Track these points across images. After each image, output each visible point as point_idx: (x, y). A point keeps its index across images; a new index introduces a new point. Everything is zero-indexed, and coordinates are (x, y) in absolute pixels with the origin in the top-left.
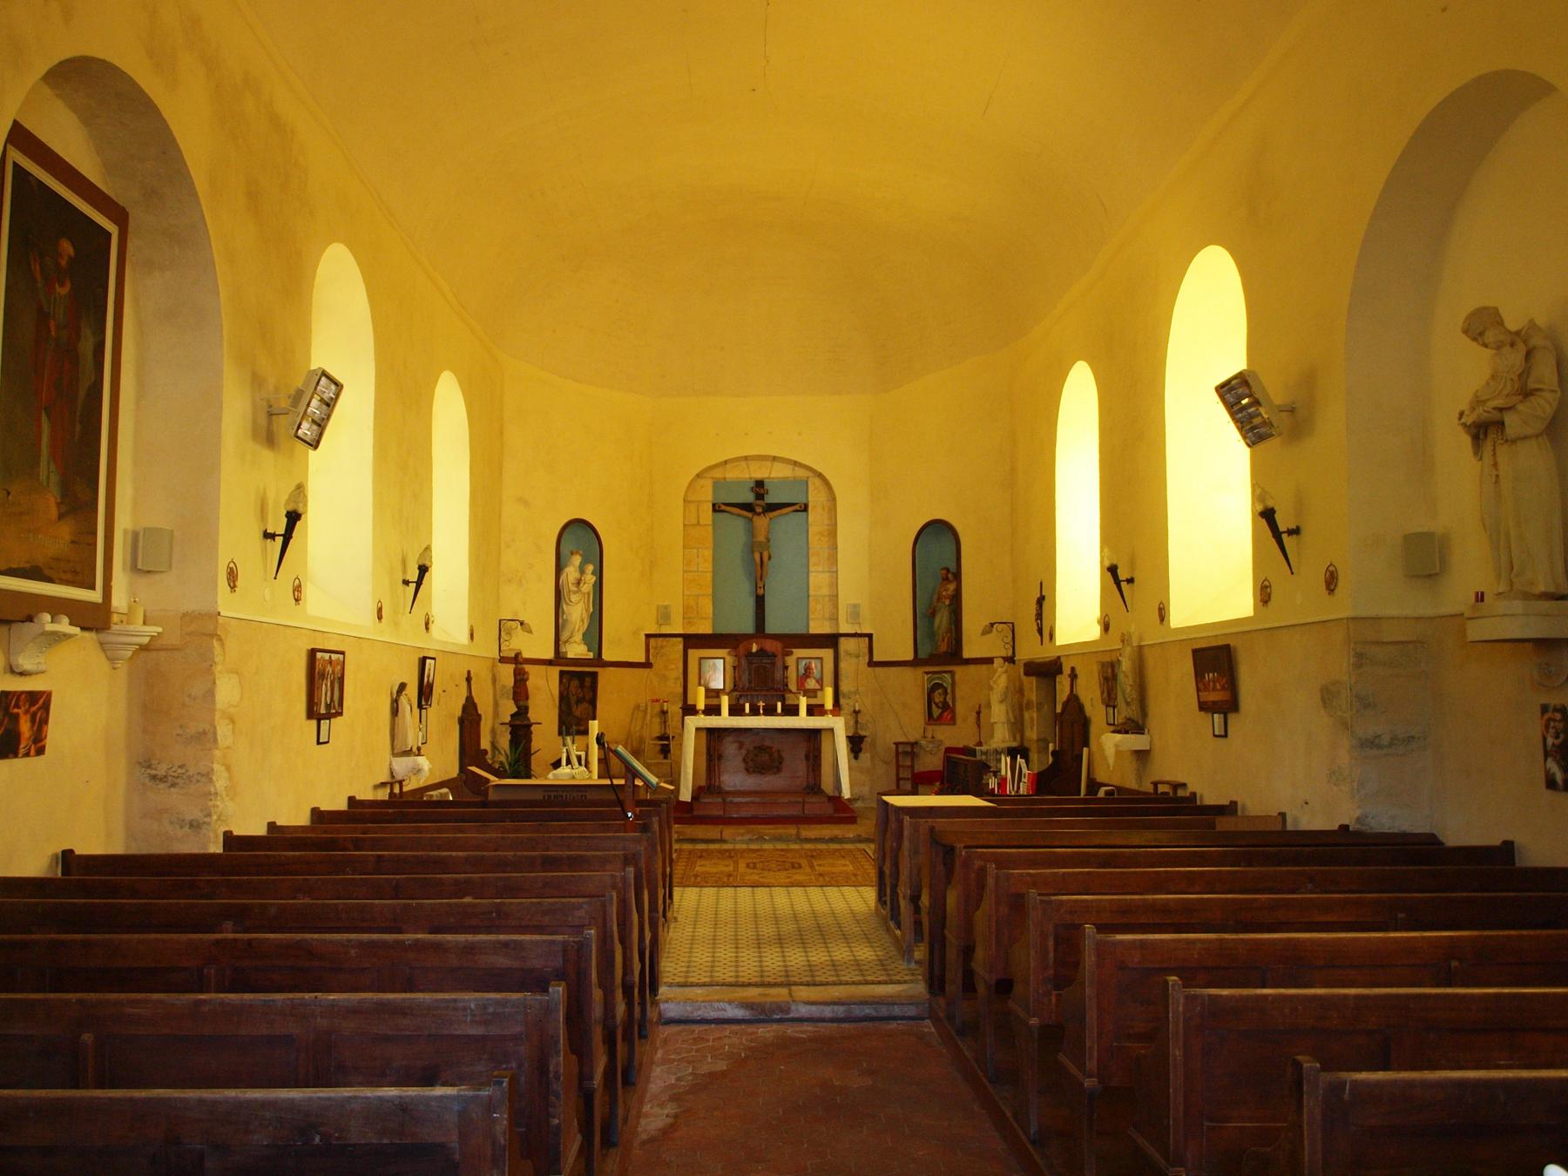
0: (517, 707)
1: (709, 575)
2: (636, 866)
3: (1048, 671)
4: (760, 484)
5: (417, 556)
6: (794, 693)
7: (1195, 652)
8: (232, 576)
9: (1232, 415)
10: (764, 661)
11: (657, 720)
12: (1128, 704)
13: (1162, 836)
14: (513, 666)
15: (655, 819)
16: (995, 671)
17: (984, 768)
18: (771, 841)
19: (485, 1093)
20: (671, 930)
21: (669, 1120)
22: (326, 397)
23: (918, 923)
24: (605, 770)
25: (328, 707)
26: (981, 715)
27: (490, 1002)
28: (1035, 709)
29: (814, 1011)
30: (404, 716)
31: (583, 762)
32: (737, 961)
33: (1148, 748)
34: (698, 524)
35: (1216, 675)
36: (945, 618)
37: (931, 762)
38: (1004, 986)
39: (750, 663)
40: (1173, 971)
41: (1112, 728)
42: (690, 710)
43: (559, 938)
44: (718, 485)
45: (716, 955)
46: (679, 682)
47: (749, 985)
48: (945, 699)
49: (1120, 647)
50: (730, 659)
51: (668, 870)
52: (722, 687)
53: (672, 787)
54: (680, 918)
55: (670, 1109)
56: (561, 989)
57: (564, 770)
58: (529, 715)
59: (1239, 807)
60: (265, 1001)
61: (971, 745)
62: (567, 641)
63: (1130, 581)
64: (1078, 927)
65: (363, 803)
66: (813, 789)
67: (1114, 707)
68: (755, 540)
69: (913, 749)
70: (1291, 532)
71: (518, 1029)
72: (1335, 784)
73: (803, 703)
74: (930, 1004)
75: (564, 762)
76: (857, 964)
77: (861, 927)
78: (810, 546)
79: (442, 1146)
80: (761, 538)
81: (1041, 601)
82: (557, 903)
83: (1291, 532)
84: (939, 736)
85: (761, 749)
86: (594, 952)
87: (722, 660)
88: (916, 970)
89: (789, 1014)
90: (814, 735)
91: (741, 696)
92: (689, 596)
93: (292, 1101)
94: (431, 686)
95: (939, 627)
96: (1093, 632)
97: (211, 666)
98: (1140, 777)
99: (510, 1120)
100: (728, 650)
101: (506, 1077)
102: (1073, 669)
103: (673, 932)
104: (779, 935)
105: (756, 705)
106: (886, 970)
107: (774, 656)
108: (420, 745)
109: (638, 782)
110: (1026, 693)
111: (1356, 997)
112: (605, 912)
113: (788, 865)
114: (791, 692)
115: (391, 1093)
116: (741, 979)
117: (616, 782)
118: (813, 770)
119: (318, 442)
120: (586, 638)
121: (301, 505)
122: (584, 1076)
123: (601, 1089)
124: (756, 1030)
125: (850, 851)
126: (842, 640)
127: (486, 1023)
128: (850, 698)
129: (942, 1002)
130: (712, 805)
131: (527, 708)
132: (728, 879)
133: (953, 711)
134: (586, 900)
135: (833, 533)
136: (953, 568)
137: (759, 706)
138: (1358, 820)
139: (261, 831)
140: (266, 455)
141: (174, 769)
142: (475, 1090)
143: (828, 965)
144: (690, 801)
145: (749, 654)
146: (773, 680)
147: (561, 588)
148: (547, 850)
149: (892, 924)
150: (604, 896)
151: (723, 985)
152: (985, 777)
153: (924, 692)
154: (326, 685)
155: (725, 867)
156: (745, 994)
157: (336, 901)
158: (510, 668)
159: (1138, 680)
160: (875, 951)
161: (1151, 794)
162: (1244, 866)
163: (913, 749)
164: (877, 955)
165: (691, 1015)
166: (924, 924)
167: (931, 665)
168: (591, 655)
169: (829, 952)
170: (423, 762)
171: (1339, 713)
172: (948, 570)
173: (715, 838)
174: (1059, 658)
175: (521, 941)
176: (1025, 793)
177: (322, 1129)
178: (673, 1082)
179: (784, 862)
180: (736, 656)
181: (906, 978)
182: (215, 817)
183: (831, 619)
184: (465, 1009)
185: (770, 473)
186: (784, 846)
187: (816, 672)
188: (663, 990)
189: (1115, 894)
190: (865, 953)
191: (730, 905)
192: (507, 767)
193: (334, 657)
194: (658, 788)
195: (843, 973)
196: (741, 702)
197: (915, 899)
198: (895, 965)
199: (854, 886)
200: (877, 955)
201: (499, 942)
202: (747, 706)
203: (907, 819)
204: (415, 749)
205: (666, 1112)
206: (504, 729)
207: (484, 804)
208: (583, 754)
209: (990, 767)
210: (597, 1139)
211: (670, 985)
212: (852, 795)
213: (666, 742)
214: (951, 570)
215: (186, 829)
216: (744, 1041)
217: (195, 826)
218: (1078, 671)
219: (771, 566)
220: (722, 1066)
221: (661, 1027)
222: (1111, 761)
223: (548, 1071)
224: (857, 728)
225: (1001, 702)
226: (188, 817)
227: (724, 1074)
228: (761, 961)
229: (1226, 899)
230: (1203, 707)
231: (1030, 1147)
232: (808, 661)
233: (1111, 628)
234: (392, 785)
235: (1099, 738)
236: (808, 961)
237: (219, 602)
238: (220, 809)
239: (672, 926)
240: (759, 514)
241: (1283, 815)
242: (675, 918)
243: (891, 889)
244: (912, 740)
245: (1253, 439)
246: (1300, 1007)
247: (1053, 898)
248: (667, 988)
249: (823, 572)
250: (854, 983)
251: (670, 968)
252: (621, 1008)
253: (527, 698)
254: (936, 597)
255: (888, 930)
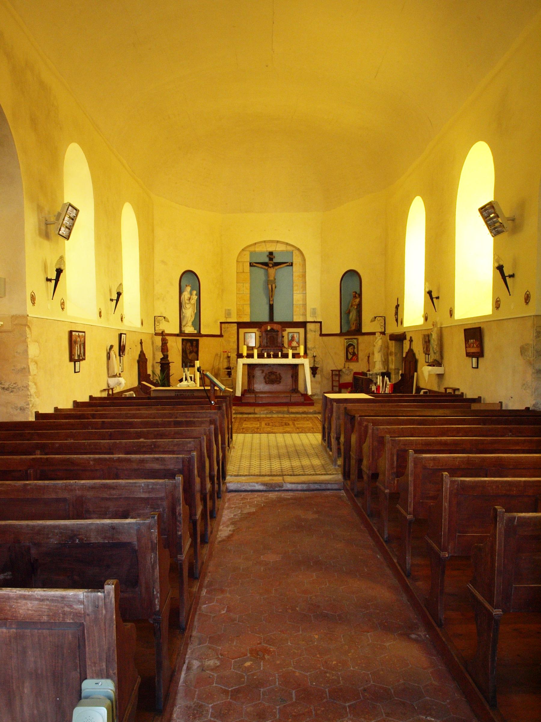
0: (164, 355)
1: (248, 295)
2: (215, 425)
3: (399, 338)
4: (271, 253)
5: (116, 288)
6: (286, 348)
7: (465, 330)
8: (33, 298)
9: (486, 222)
10: (273, 334)
11: (226, 360)
12: (435, 353)
13: (447, 411)
14: (161, 337)
15: (224, 404)
16: (376, 338)
17: (370, 381)
18: (276, 413)
19: (148, 521)
20: (232, 452)
21: (231, 533)
22: (72, 216)
23: (339, 449)
24: (203, 384)
25: (79, 356)
26: (370, 358)
27: (150, 484)
28: (394, 355)
29: (293, 486)
30: (113, 359)
31: (193, 379)
32: (260, 465)
33: (443, 373)
34: (243, 272)
35: (474, 340)
36: (354, 315)
37: (348, 378)
38: (375, 476)
39: (267, 335)
40: (445, 470)
41: (427, 364)
42: (240, 356)
43: (181, 456)
44: (252, 254)
45: (251, 463)
46: (235, 343)
47: (265, 475)
48: (354, 351)
49: (432, 328)
50: (258, 333)
51: (230, 426)
52: (254, 346)
53: (231, 390)
54: (236, 447)
55: (231, 528)
56: (180, 478)
57: (184, 383)
58: (169, 359)
59: (482, 399)
60: (54, 484)
61: (365, 371)
62: (185, 326)
63: (438, 298)
64: (407, 451)
65: (96, 398)
66: (295, 391)
67: (429, 355)
68: (269, 279)
69: (339, 373)
70: (510, 276)
71: (163, 495)
72: (524, 390)
73: (290, 352)
74: (344, 483)
75: (184, 379)
76: (313, 467)
77: (315, 451)
78: (294, 282)
79: (130, 544)
80: (272, 278)
81: (397, 307)
82: (180, 441)
83: (510, 276)
84: (351, 367)
85: (272, 373)
86: (196, 462)
87: (254, 334)
88: (338, 469)
89: (283, 488)
90: (295, 367)
91: (263, 349)
92: (239, 305)
93: (66, 525)
94: (124, 346)
95: (352, 318)
96: (420, 321)
97: (26, 339)
98: (439, 386)
99: (159, 532)
100: (257, 329)
101: (156, 515)
102: (411, 337)
103: (233, 453)
104: (279, 454)
105: (269, 353)
106: (325, 469)
107: (278, 331)
108: (120, 372)
109: (216, 388)
110: (390, 348)
111: (525, 481)
112: (201, 444)
113: (284, 424)
114: (285, 347)
115: (108, 522)
116: (262, 473)
117: (206, 388)
118: (295, 381)
119: (69, 236)
120: (193, 324)
121: (62, 266)
122: (192, 514)
123: (200, 519)
124: (268, 495)
125: (311, 418)
126: (308, 325)
127: (149, 492)
128: (311, 350)
129: (349, 482)
130: (250, 398)
131: (167, 356)
132: (257, 430)
133: (357, 356)
134: (193, 439)
135: (304, 276)
136: (358, 292)
137: (271, 354)
138: (534, 405)
139: (52, 411)
140: (46, 243)
141: (11, 385)
142: (143, 520)
143: (300, 467)
144: (240, 396)
145: (266, 331)
146: (277, 342)
147: (182, 301)
148: (176, 418)
149: (328, 449)
150: (200, 438)
151: (254, 475)
152: (371, 385)
153: (344, 348)
154: (77, 347)
155: (256, 425)
156: (263, 479)
157: (84, 441)
158: (160, 338)
159: (439, 343)
160: (320, 461)
161: (443, 393)
162: (482, 425)
163: (339, 373)
164: (321, 463)
165: (240, 488)
166: (341, 449)
167: (348, 335)
168: (196, 332)
169: (300, 461)
170: (122, 380)
171: (528, 358)
172: (356, 293)
173: (251, 412)
174: (405, 332)
175: (164, 458)
176: (388, 393)
177: (80, 536)
178: (232, 516)
179: (282, 422)
180: (261, 332)
181: (334, 472)
182: (31, 405)
183: (303, 315)
184: (139, 486)
185: (276, 248)
186: (282, 416)
187: (296, 339)
188: (228, 478)
189: (424, 437)
190: (316, 462)
191: (258, 441)
192: (159, 382)
193: (80, 334)
194: (225, 391)
195: (306, 470)
196: (263, 352)
197: (338, 439)
198: (329, 467)
199: (305, 433)
200: (321, 463)
201: (154, 458)
202: (265, 354)
203: (335, 404)
204: (118, 375)
205: (229, 529)
206: (157, 365)
207: (149, 398)
208: (193, 376)
209: (373, 381)
210: (199, 540)
211: (231, 476)
212: (312, 393)
213: (229, 370)
214: (358, 293)
215: (19, 411)
216: (263, 499)
217: (22, 409)
218: (413, 339)
219: (277, 292)
220: (253, 510)
221: (227, 494)
222: (427, 379)
223: (176, 512)
224: (314, 364)
225: (379, 352)
226: (20, 406)
227: (254, 513)
228: (271, 466)
229: (472, 439)
230: (468, 355)
231: (384, 543)
232: (293, 333)
233: (428, 319)
234: (108, 390)
235: (422, 368)
236: (291, 465)
237: (28, 310)
238: (33, 402)
239: (232, 450)
240: (271, 267)
241: (501, 403)
242: (234, 447)
243: (328, 434)
244: (339, 369)
245: (495, 233)
246: (500, 486)
247: (397, 438)
248: (230, 477)
249: (300, 293)
250: (311, 475)
251: (231, 468)
252: (209, 486)
253: (168, 351)
254: (350, 304)
255: (326, 451)
